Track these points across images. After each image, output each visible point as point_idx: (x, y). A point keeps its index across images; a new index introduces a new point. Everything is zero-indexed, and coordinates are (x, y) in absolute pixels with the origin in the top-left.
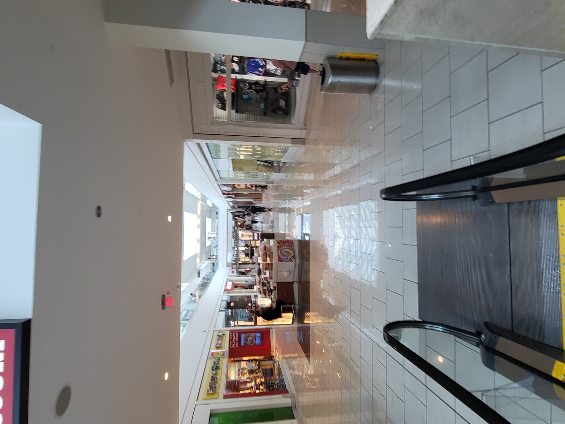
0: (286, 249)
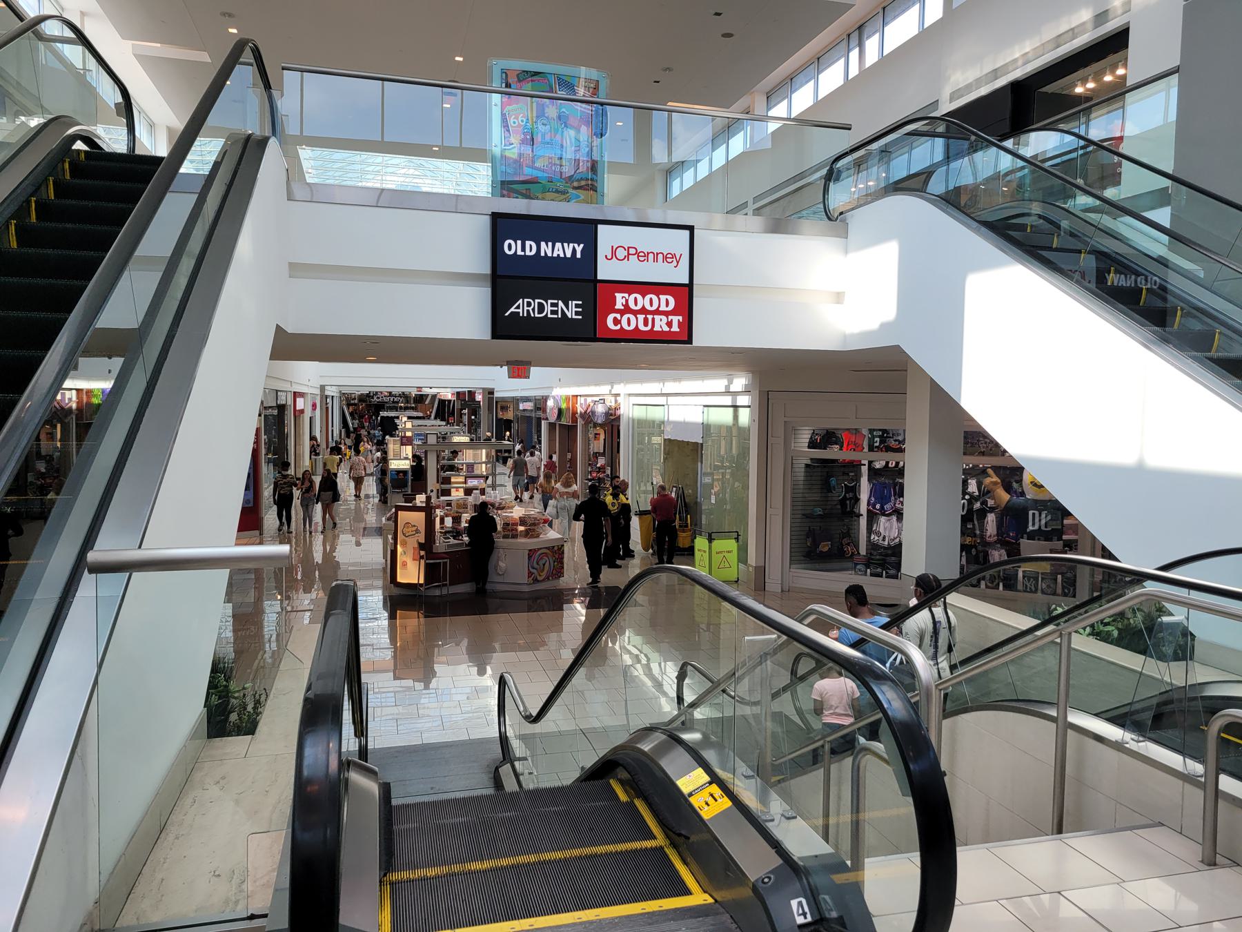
0: (548, 563)
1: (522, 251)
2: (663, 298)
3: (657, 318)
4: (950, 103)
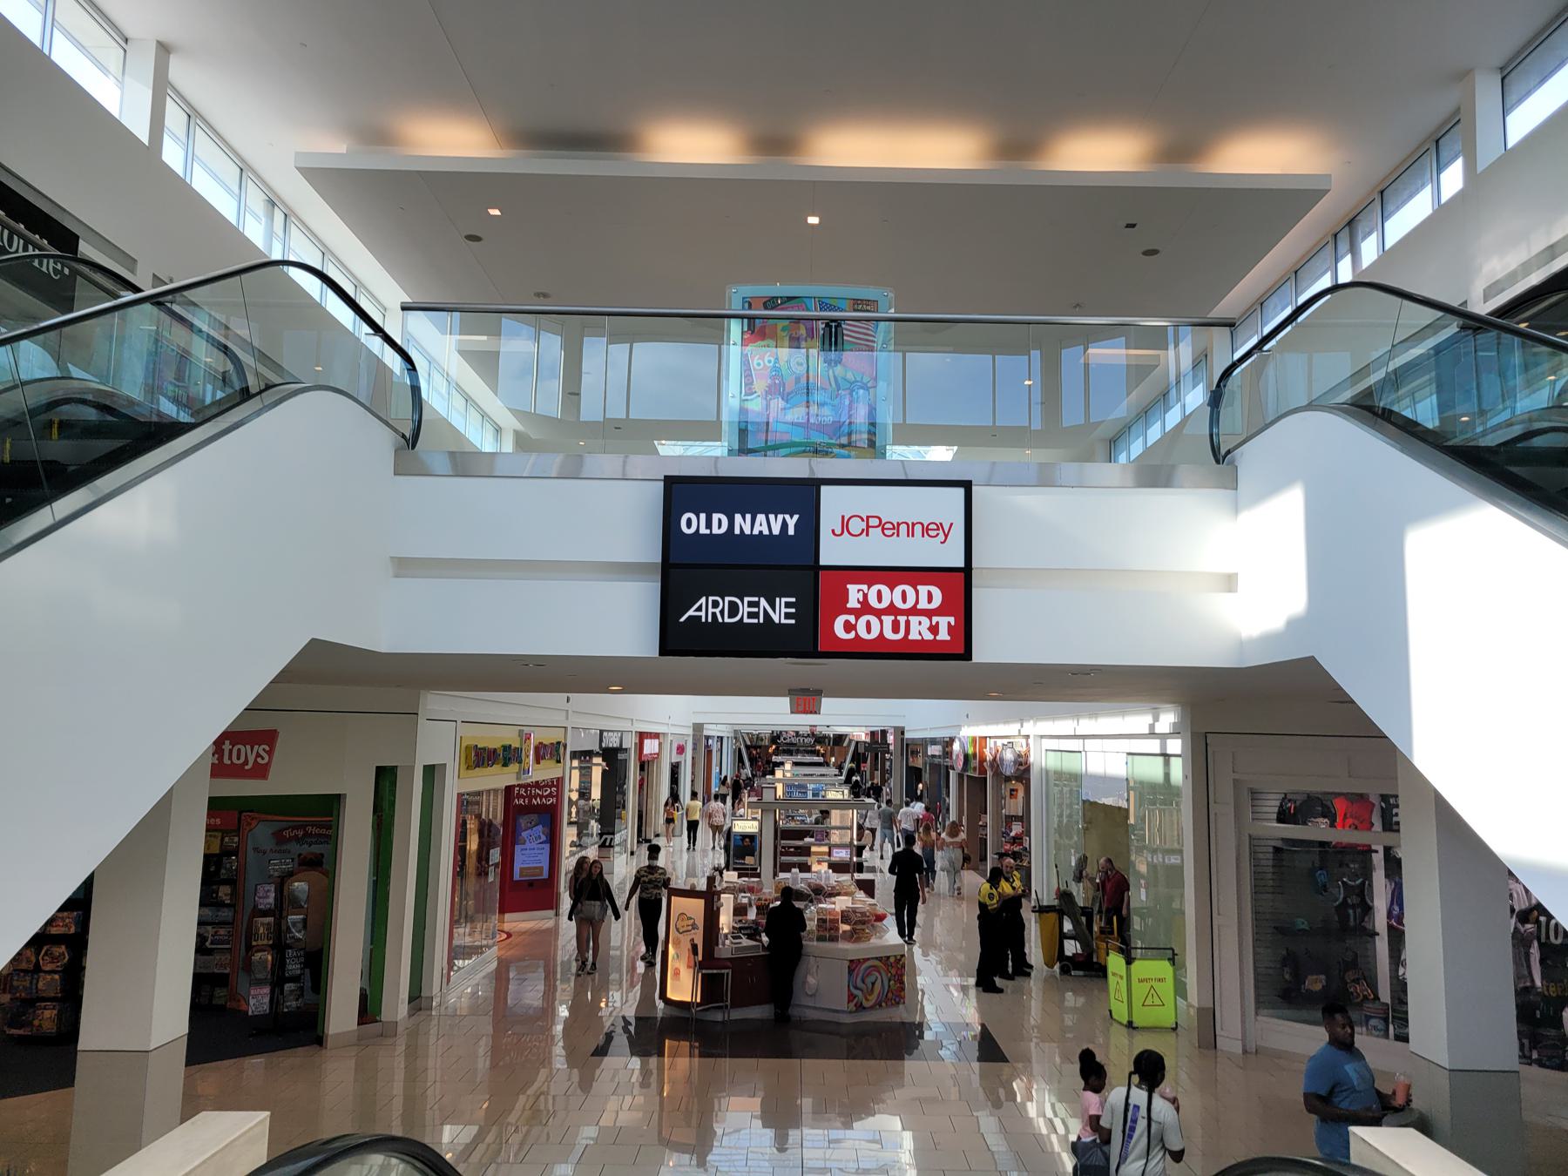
0: (880, 982)
1: (707, 528)
2: (923, 589)
3: (914, 620)
4: (1485, 302)
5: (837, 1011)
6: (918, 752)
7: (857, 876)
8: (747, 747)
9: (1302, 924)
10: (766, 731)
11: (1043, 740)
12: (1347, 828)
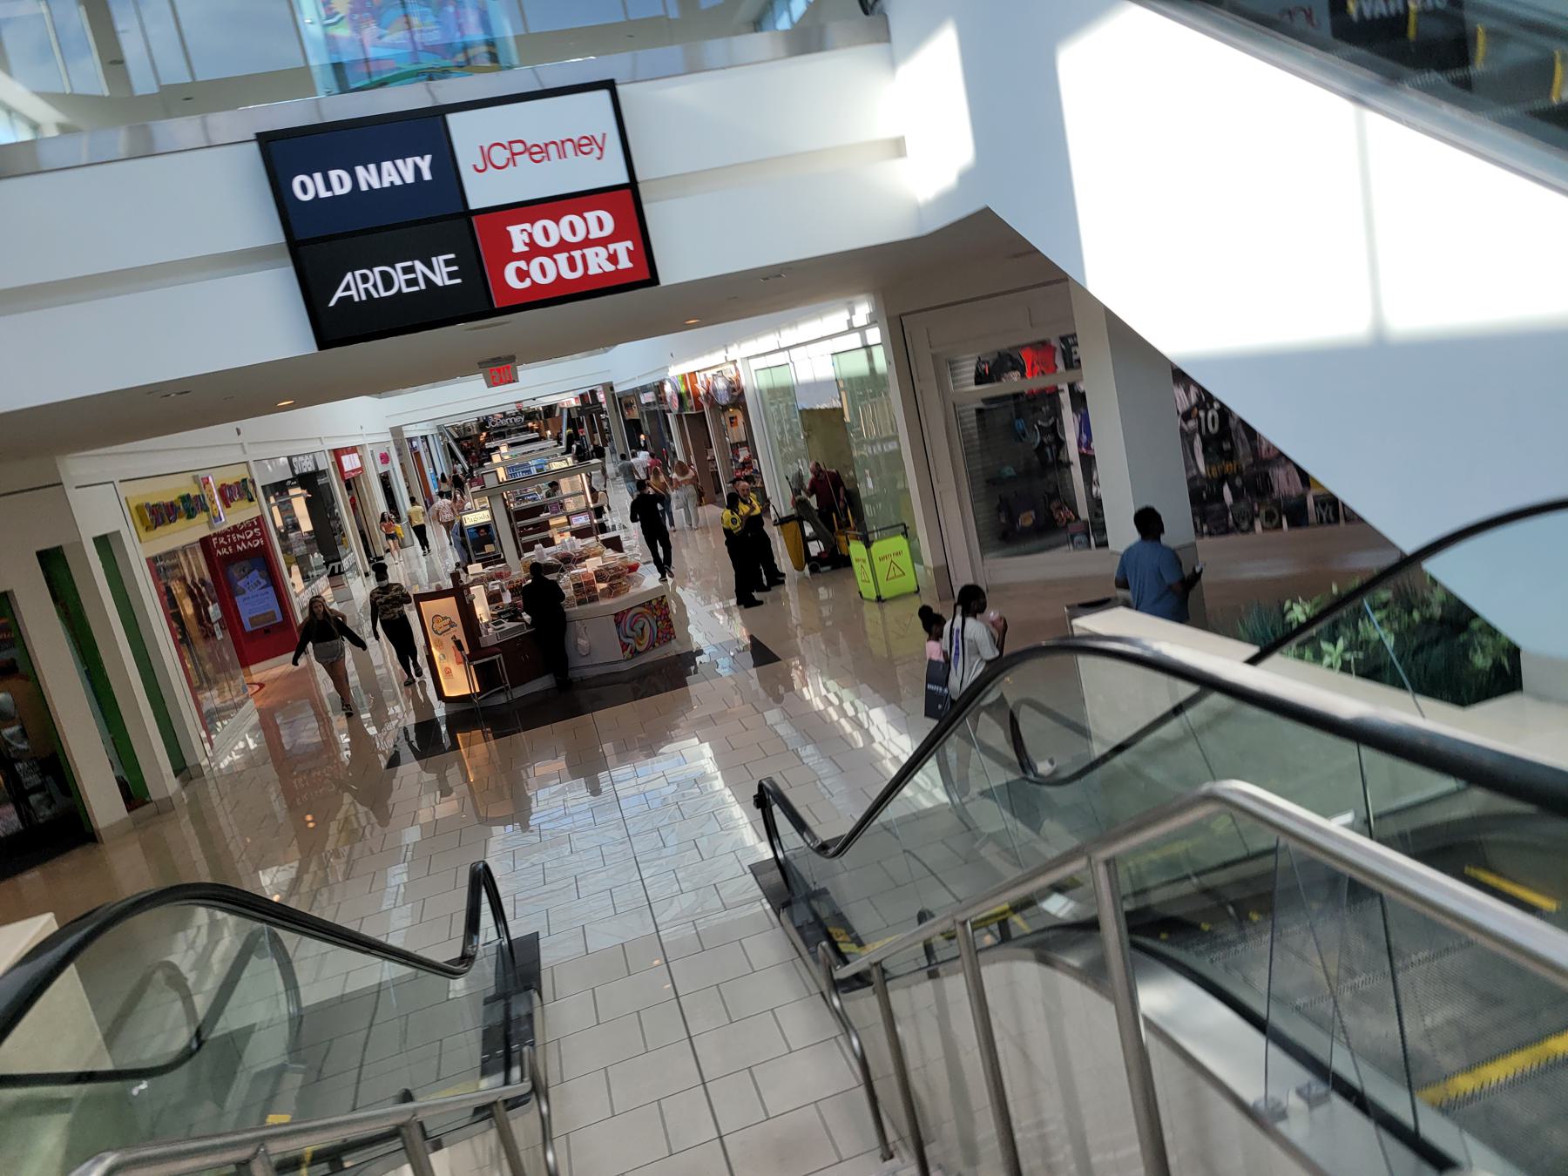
0: (648, 626)
2: (591, 216)
3: (589, 252)
5: (616, 662)
6: (632, 404)
7: (601, 537)
8: (456, 441)
9: (1009, 471)
10: (471, 419)
11: (751, 361)
12: (1036, 376)
